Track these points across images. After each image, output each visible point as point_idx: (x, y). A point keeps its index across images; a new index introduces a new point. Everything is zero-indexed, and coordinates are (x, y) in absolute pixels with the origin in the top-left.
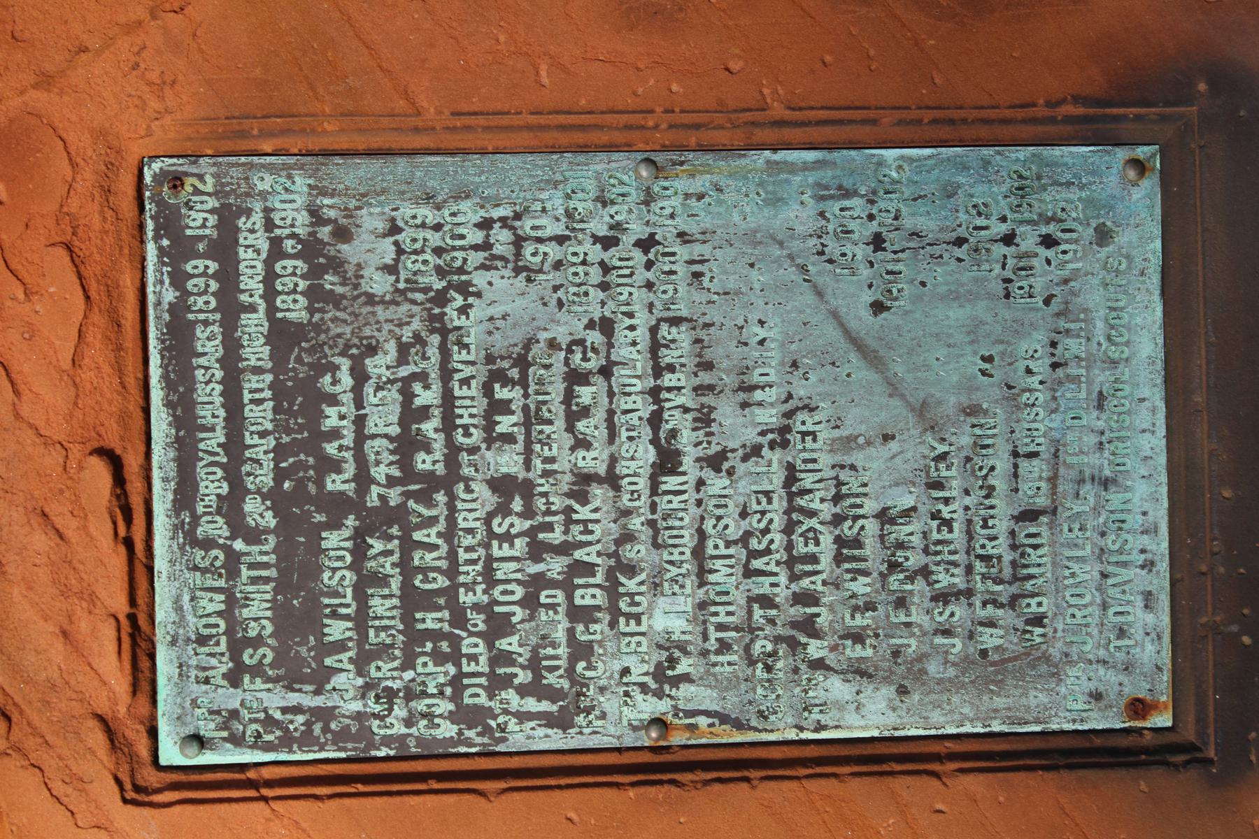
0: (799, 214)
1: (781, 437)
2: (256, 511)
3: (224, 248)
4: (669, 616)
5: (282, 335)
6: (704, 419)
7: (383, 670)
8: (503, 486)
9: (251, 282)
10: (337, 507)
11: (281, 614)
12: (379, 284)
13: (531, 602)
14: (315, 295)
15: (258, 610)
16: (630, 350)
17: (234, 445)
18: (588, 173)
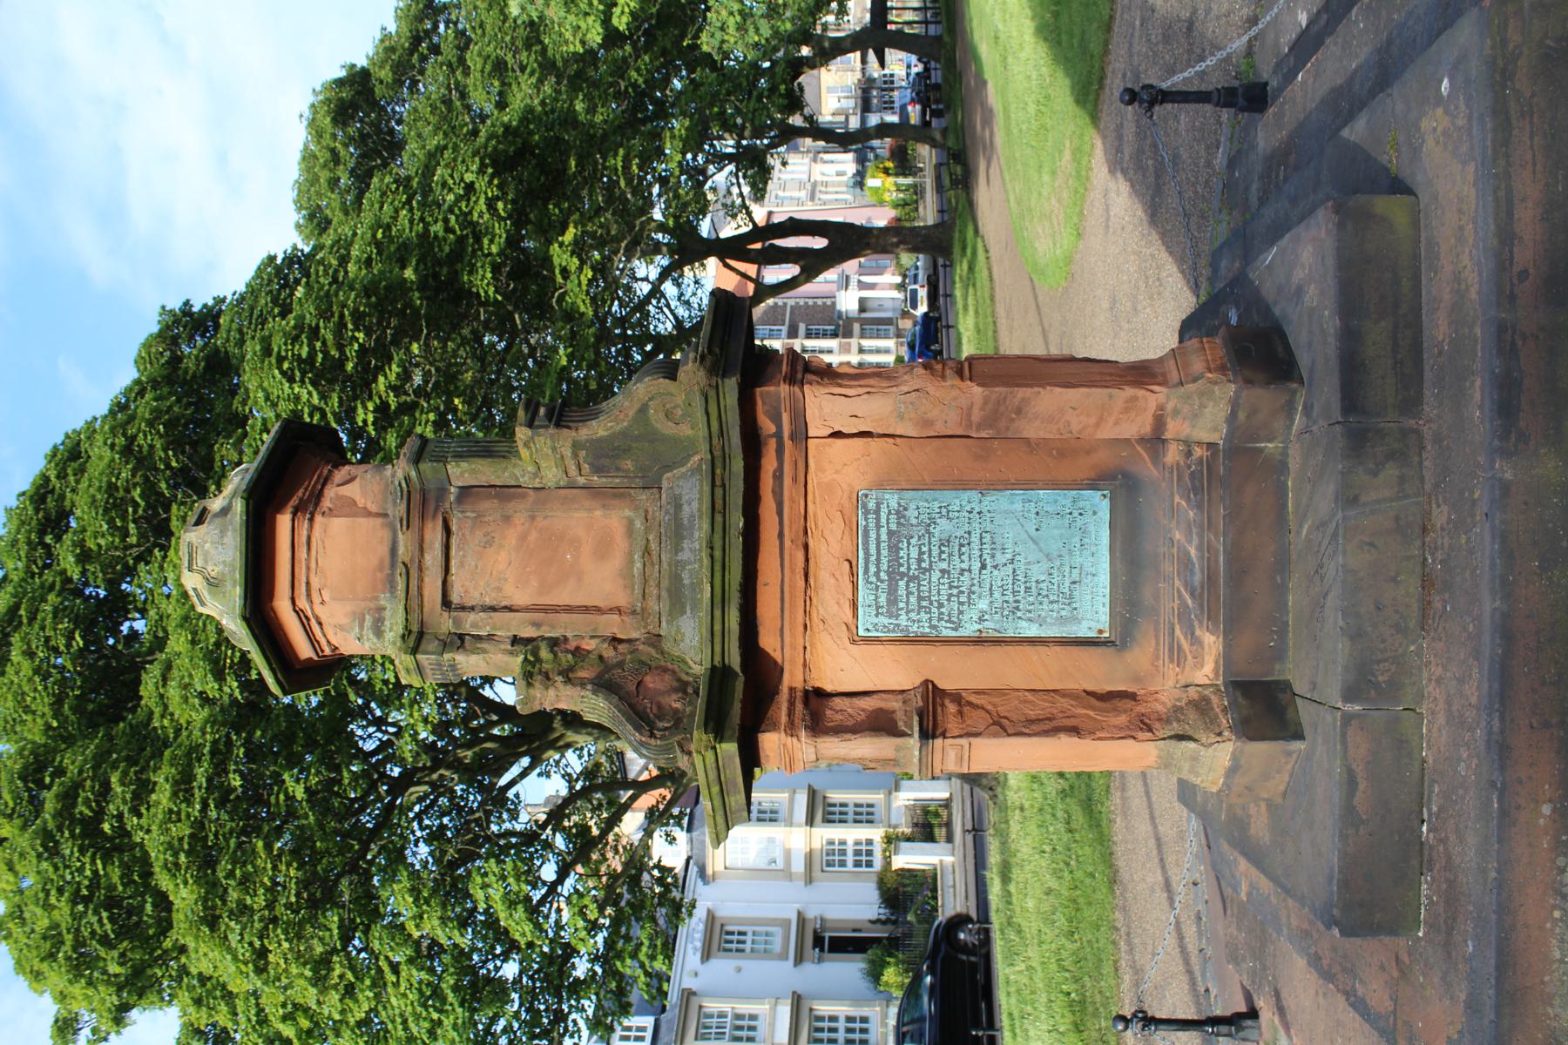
0: (1018, 506)
2: (883, 575)
3: (877, 512)
4: (983, 604)
5: (890, 533)
6: (993, 556)
7: (913, 615)
8: (943, 571)
9: (883, 520)
10: (902, 575)
11: (888, 601)
12: (914, 521)
14: (899, 524)
15: (883, 599)
16: (975, 539)
18: (966, 495)
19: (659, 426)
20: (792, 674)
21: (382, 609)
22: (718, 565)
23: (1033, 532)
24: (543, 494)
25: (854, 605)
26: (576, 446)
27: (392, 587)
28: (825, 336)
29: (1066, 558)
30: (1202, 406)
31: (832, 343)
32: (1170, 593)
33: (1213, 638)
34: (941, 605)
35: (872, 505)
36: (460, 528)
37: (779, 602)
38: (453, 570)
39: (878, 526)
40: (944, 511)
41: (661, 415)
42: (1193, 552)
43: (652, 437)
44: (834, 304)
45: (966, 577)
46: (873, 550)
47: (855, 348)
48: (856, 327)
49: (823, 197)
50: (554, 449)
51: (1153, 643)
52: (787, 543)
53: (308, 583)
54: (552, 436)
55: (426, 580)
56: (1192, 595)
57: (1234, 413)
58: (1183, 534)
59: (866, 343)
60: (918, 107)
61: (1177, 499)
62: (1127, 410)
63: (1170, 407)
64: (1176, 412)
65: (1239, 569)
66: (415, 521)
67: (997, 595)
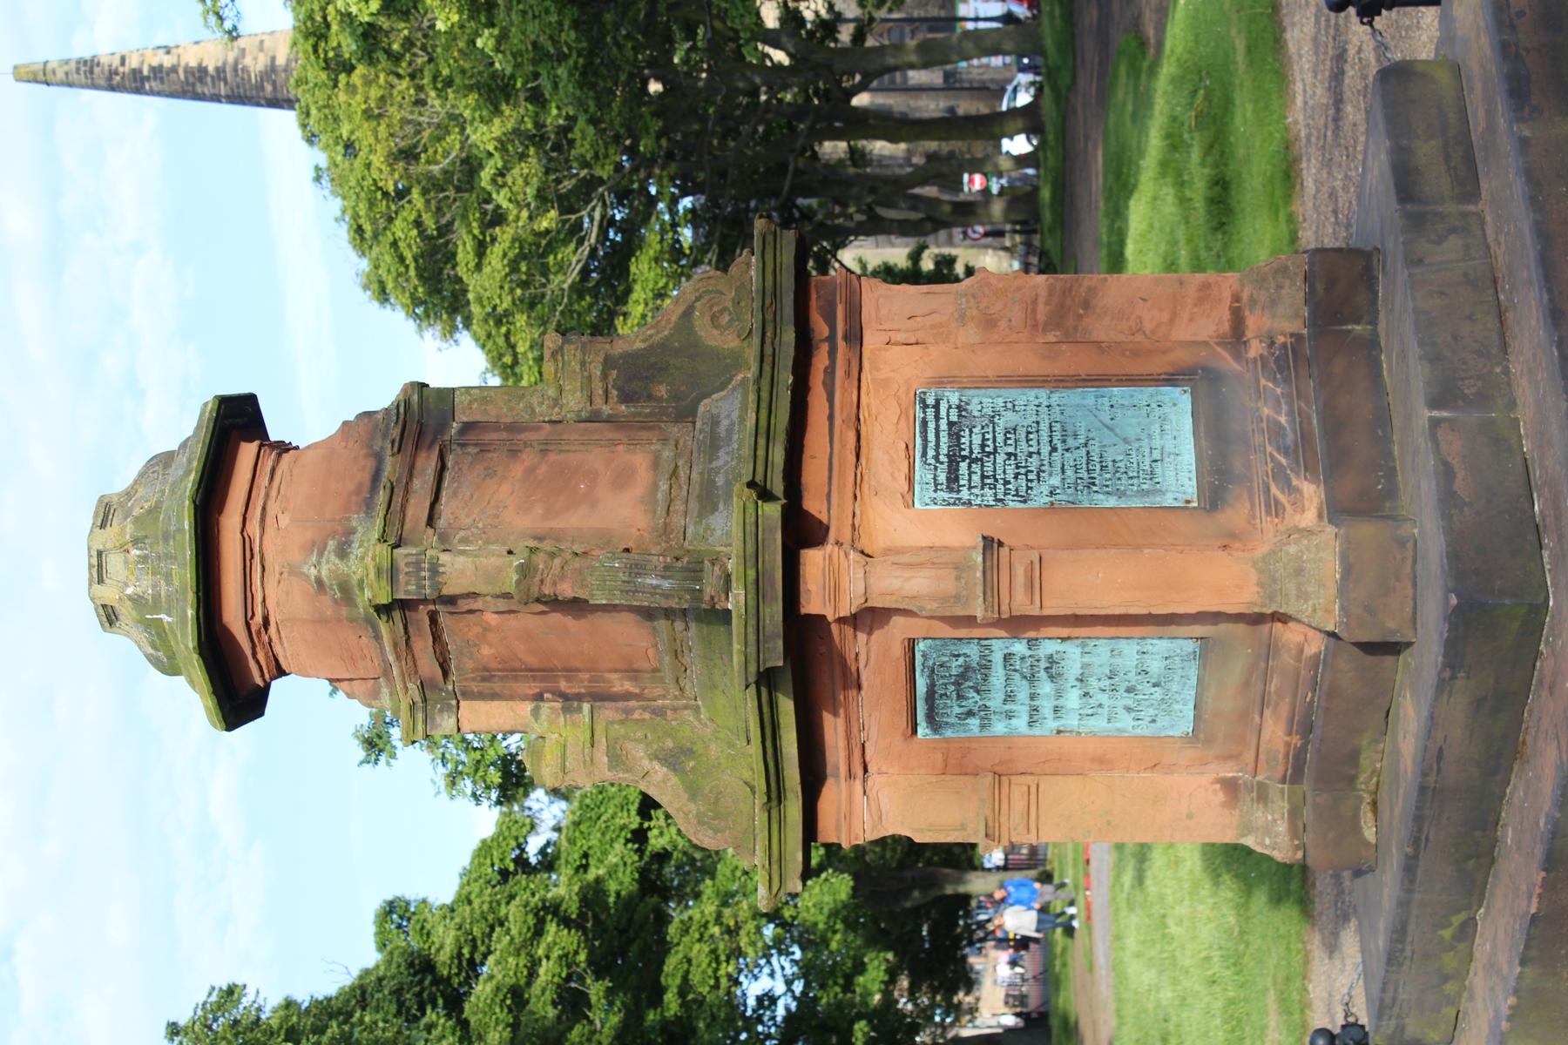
0: (1090, 401)
1: (1086, 445)
2: (943, 458)
3: (937, 406)
4: (1055, 481)
5: (951, 424)
6: (1064, 441)
7: (975, 491)
8: (1009, 455)
9: (943, 413)
10: (964, 458)
11: (948, 479)
12: (976, 414)
13: (1016, 478)
14: (960, 416)
15: (942, 478)
16: (1044, 427)
17: (937, 445)
18: (1031, 393)
19: (701, 333)
20: (838, 531)
21: (353, 531)
23: (1107, 420)
24: (559, 426)
25: (910, 480)
26: (609, 363)
27: (369, 506)
29: (1145, 443)
30: (1279, 287)
32: (1263, 458)
33: (1312, 488)
34: (1006, 483)
35: (931, 401)
36: (457, 463)
37: (826, 473)
38: (443, 500)
39: (937, 418)
40: (1009, 405)
41: (707, 319)
42: (1283, 419)
43: (694, 350)
45: (1034, 460)
46: (931, 437)
50: (583, 364)
51: (1248, 505)
52: (838, 421)
53: (264, 509)
54: (584, 345)
55: (412, 501)
56: (1286, 454)
57: (1312, 288)
58: (1269, 408)
61: (1263, 382)
62: (1200, 301)
63: (1245, 296)
64: (1253, 302)
65: (1334, 426)
66: (409, 446)
67: (1069, 472)
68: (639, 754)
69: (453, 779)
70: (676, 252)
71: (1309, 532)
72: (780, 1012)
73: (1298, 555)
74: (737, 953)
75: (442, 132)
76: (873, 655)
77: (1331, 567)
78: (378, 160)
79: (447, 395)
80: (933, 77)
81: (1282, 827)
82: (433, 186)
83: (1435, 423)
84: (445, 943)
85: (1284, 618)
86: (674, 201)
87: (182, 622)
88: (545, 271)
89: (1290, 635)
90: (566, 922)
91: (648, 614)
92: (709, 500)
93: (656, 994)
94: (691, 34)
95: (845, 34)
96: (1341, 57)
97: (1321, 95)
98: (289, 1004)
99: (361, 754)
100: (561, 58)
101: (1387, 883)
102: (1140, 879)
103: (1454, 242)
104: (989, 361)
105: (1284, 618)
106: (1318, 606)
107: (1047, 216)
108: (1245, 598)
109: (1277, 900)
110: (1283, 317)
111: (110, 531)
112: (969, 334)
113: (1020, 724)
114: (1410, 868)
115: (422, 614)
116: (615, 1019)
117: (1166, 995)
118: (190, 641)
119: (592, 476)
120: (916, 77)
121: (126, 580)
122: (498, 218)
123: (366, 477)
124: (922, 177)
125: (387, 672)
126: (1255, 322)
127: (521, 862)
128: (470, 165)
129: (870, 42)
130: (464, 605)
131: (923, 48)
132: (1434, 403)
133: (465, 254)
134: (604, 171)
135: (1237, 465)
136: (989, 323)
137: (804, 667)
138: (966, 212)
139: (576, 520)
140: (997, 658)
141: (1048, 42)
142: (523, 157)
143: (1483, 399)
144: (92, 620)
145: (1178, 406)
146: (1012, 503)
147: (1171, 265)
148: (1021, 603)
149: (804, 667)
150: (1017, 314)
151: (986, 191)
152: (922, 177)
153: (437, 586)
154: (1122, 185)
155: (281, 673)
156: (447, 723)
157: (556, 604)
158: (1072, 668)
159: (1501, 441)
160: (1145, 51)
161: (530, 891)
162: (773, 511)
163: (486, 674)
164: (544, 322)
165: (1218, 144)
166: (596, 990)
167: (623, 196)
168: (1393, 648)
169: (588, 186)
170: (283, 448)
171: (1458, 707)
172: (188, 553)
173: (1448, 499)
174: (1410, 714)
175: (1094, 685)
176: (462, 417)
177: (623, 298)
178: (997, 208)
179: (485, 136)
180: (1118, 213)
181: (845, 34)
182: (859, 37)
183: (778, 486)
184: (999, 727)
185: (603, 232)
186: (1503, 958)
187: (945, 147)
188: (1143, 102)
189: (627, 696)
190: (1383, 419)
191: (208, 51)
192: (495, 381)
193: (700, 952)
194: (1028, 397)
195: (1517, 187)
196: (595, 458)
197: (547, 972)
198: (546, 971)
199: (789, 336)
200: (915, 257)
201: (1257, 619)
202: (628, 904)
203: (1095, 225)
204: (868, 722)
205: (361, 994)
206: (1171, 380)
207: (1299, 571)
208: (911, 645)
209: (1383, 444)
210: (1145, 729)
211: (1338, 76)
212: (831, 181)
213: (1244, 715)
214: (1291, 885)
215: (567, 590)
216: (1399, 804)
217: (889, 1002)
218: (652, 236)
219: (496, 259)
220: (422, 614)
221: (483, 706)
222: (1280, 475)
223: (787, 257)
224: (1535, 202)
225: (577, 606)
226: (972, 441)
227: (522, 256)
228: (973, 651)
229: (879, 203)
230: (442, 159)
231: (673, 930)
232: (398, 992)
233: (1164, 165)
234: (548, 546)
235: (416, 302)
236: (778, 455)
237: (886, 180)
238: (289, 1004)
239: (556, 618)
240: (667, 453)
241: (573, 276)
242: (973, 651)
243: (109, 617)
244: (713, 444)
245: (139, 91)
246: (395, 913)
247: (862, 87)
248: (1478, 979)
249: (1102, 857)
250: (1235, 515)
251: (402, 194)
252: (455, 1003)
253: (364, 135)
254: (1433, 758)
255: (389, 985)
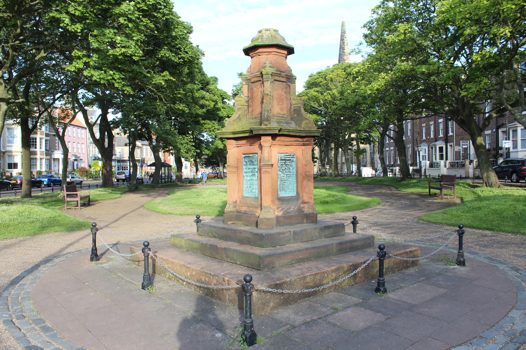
22: (293, 131)
26: (299, 107)
27: (277, 71)
28: (46, 146)
31: (44, 149)
32: (285, 206)
43: (302, 120)
44: (56, 150)
47: (42, 157)
48: (49, 157)
49: (91, 147)
58: (293, 208)
59: (44, 161)
60: (124, 178)
62: (309, 197)
65: (290, 217)
68: (240, 112)
69: (235, 86)
70: (317, 121)
71: (274, 213)
72: (201, 138)
73: (271, 212)
74: (210, 132)
75: (335, 85)
76: (255, 148)
77: (269, 216)
78: (331, 76)
79: (294, 83)
80: (344, 161)
81: (230, 210)
82: (327, 84)
83: (291, 232)
84: (211, 87)
85: (261, 210)
86: (325, 121)
87: (259, 43)
88: (314, 101)
89: (259, 211)
90: (215, 105)
91: (261, 113)
92: (278, 123)
93: (204, 119)
94: (350, 124)
95: (350, 147)
96: (346, 220)
97: (340, 217)
98: (202, 63)
99: (239, 73)
100: (346, 103)
101: (221, 225)
102: (221, 191)
103: (318, 235)
104: (300, 165)
105: (261, 210)
106: (263, 215)
107: (323, 178)
108: (264, 204)
109: (219, 211)
110: (307, 210)
111: (273, 32)
112: (304, 162)
113: (245, 170)
114: (224, 228)
115: (261, 79)
116: (200, 113)
117: (205, 195)
118: (256, 44)
119: (282, 105)
120: (344, 158)
121: (266, 34)
122: (322, 94)
123: (282, 70)
124: (329, 159)
125: (252, 74)
126: (306, 205)
127: (223, 99)
128: (330, 90)
129: (349, 151)
130: (262, 85)
131: (348, 159)
132: (294, 232)
133: (316, 89)
134: (329, 110)
135: (284, 203)
136: (306, 165)
137: (253, 137)
138: (323, 165)
139: (275, 102)
140: (255, 167)
141: (349, 178)
142: (332, 98)
143: (294, 239)
144: (260, 29)
145: (294, 194)
146: (278, 169)
147: (315, 196)
148: (263, 170)
149: (253, 137)
150: (307, 169)
151: (326, 169)
152: (329, 159)
153: (265, 81)
154: (327, 188)
155: (252, 58)
156: (244, 83)
157: (263, 99)
158: (254, 178)
159: (288, 241)
160: (348, 192)
161: (219, 100)
162: (277, 132)
163: (252, 89)
164: (306, 101)
165: (333, 202)
166: (204, 110)
167: (326, 113)
168: (257, 226)
169: (327, 108)
170: (286, 58)
171: (249, 235)
172: (270, 43)
173: (279, 234)
174: (247, 228)
175: (251, 181)
176: (291, 85)
177: (310, 113)
178: (324, 170)
179: (335, 91)
180: (323, 188)
181: (350, 147)
182: (350, 149)
183: (281, 133)
184: (244, 167)
185: (320, 110)
186: (211, 242)
187: (333, 163)
188: (340, 191)
189: (248, 111)
190: (292, 225)
191: (347, 50)
192: (297, 94)
193: (210, 126)
194: (295, 171)
195: (326, 244)
196: (285, 105)
197: (207, 103)
198: (207, 103)
199: (304, 135)
200: (316, 158)
201: (261, 206)
202: (217, 115)
203: (321, 185)
204: (245, 147)
205: (203, 74)
206: (297, 193)
207: (268, 212)
208: (257, 154)
209: (288, 224)
210: (244, 189)
211: (343, 219)
212: (328, 145)
213: (246, 204)
214: (221, 213)
215: (264, 101)
216: (234, 227)
217: (203, 155)
218: (318, 118)
219: (315, 94)
220: (261, 79)
221: (247, 89)
222: (283, 209)
223: (316, 134)
224: (323, 246)
225: (262, 102)
226: (288, 162)
227: (316, 98)
228: (256, 163)
229: (325, 152)
230: (331, 85)
231: (214, 121)
232: (204, 80)
233: (330, 194)
234: (271, 98)
235: (309, 82)
236: (285, 133)
237: (328, 153)
238: (202, 63)
239: (260, 99)
240: (286, 116)
241: (313, 106)
242: (256, 163)
243: (260, 32)
244: (287, 123)
245: (341, 40)
246: (216, 79)
247: (342, 150)
248: (208, 238)
249: (225, 186)
250: (277, 202)
251: (326, 80)
252: (202, 89)
253: (334, 74)
254: (241, 232)
255: (205, 79)
